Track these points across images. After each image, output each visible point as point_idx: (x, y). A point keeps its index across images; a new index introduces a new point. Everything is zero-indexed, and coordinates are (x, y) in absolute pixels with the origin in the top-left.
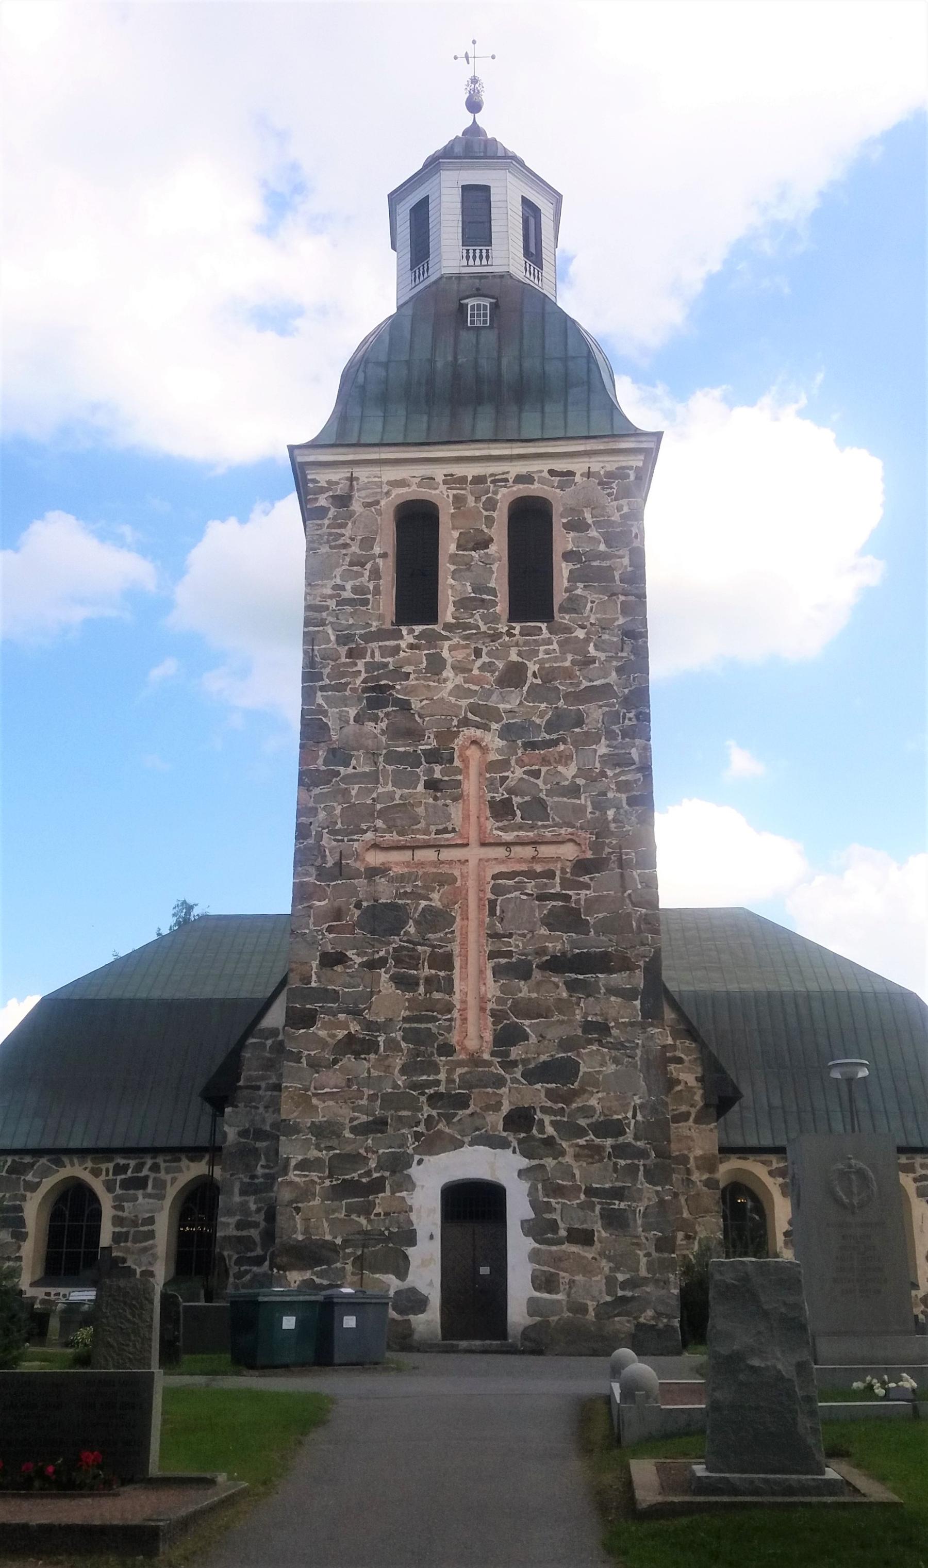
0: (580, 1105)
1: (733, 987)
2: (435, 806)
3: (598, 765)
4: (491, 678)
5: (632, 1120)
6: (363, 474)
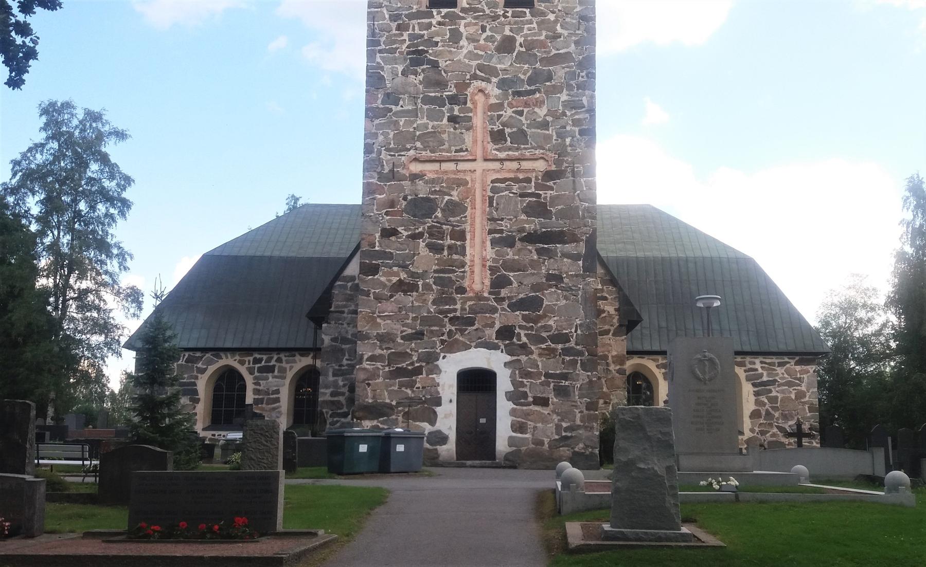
1: (640, 254)
3: (561, 108)
5: (575, 333)
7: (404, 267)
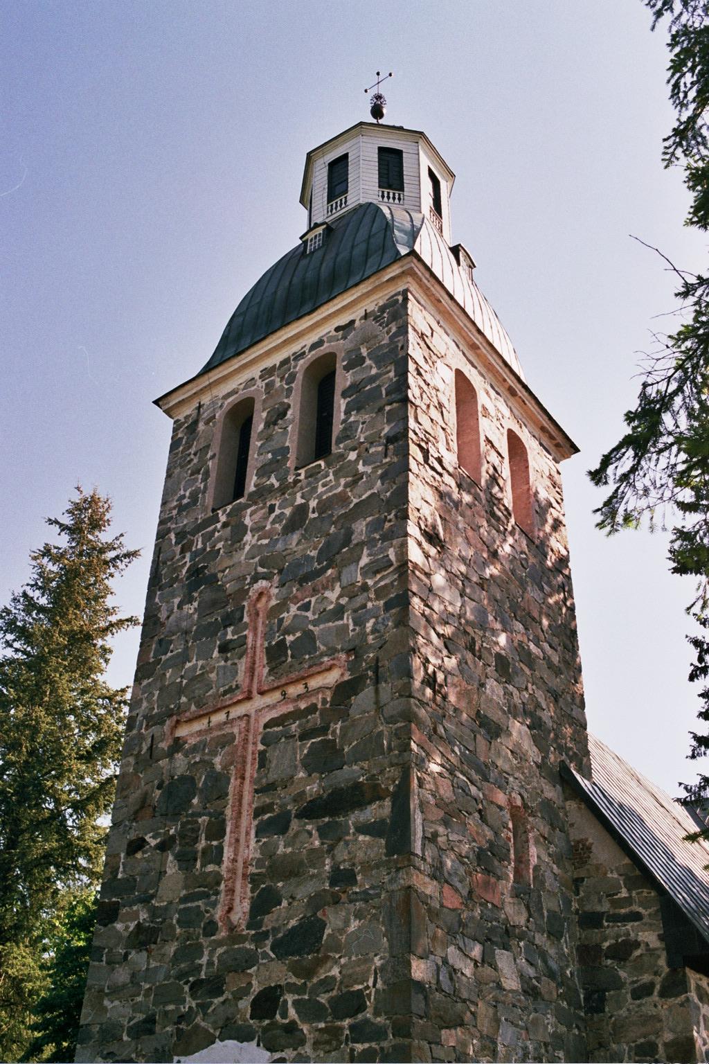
0: (323, 977)
2: (224, 667)
3: (359, 578)
4: (278, 527)
5: (372, 986)
6: (206, 399)
7: (146, 900)
